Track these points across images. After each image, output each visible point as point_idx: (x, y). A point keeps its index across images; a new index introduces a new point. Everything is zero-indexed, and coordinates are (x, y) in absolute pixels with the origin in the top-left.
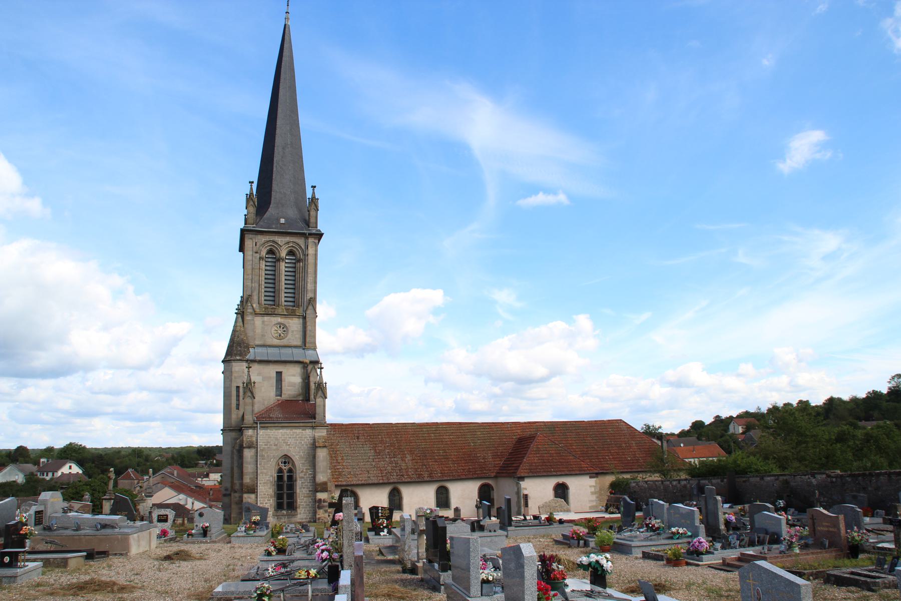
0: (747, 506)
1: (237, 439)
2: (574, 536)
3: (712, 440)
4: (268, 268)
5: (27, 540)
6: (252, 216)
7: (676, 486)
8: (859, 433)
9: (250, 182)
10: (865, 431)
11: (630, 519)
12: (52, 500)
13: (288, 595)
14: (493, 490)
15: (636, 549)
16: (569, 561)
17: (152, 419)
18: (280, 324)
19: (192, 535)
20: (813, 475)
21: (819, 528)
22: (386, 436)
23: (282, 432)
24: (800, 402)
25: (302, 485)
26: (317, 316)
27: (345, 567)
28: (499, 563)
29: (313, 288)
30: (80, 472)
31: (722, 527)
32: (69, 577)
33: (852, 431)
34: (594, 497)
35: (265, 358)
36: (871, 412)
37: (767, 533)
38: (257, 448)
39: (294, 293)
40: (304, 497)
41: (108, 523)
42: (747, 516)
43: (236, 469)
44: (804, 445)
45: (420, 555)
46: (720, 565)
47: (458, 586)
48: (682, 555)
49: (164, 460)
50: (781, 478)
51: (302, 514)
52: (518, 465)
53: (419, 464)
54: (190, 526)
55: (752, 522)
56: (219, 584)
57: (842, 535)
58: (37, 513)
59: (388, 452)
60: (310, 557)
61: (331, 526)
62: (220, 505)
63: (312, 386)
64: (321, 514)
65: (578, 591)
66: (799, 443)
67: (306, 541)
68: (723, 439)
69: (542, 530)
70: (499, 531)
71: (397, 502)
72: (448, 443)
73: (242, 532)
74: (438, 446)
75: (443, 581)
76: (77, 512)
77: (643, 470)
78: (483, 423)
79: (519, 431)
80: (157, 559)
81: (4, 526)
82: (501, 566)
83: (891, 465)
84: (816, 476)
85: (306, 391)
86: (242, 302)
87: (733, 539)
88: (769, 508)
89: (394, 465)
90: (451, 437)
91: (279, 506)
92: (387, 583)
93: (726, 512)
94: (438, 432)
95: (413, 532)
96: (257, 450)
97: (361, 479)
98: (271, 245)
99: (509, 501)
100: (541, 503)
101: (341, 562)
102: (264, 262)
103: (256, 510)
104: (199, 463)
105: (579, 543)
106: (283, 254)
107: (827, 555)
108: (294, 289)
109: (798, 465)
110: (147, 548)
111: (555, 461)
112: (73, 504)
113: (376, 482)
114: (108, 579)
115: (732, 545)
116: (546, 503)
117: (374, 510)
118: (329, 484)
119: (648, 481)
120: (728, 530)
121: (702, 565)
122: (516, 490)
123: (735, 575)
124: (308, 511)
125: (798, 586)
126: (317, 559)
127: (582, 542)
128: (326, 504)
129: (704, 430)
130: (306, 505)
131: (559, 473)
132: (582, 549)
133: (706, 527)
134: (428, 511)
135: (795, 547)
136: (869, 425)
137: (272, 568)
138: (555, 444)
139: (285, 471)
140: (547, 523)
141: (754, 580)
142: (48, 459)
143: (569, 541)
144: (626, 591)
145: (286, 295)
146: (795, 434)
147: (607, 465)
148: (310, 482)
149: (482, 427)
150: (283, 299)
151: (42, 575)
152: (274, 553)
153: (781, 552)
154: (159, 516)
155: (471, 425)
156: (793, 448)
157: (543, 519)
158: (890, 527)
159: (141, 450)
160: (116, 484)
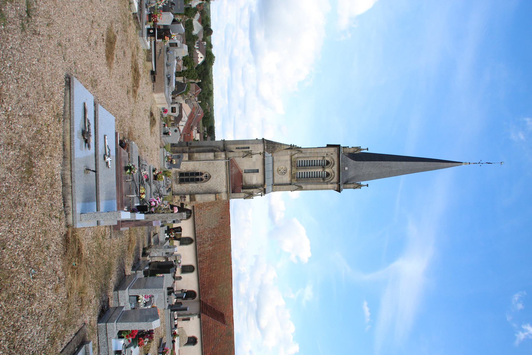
1: (219, 148)
5: (161, 40)
6: (348, 151)
12: (183, 51)
13: (130, 183)
14: (193, 299)
16: (150, 348)
17: (229, 99)
18: (286, 170)
25: (193, 187)
28: (149, 305)
29: (308, 189)
30: (199, 63)
32: (142, 63)
35: (266, 163)
38: (214, 160)
39: (305, 178)
40: (187, 188)
43: (202, 149)
45: (154, 258)
49: (207, 108)
51: (177, 187)
52: (208, 314)
58: (176, 44)
60: (152, 194)
61: (170, 205)
62: (182, 140)
63: (251, 191)
64: (177, 198)
67: (161, 191)
69: (168, 330)
71: (185, 242)
72: (220, 272)
73: (167, 154)
74: (218, 266)
76: (177, 64)
78: (232, 292)
79: (228, 314)
80: (151, 109)
85: (248, 187)
86: (298, 148)
89: (206, 240)
90: (223, 273)
91: (181, 174)
92: (137, 239)
94: (226, 265)
96: (213, 160)
97: (198, 220)
100: (184, 328)
101: (149, 213)
102: (321, 159)
106: (327, 170)
108: (307, 177)
113: (196, 229)
114: (140, 84)
116: (185, 332)
117: (179, 229)
118: (194, 202)
122: (193, 313)
131: (203, 339)
134: (179, 261)
137: (146, 173)
138: (220, 337)
139: (201, 177)
140: (172, 333)
142: (206, 46)
148: (195, 191)
149: (230, 292)
150: (301, 171)
151: (143, 49)
152: (154, 173)
154: (175, 108)
155: (231, 285)
159: (212, 95)
160: (192, 83)
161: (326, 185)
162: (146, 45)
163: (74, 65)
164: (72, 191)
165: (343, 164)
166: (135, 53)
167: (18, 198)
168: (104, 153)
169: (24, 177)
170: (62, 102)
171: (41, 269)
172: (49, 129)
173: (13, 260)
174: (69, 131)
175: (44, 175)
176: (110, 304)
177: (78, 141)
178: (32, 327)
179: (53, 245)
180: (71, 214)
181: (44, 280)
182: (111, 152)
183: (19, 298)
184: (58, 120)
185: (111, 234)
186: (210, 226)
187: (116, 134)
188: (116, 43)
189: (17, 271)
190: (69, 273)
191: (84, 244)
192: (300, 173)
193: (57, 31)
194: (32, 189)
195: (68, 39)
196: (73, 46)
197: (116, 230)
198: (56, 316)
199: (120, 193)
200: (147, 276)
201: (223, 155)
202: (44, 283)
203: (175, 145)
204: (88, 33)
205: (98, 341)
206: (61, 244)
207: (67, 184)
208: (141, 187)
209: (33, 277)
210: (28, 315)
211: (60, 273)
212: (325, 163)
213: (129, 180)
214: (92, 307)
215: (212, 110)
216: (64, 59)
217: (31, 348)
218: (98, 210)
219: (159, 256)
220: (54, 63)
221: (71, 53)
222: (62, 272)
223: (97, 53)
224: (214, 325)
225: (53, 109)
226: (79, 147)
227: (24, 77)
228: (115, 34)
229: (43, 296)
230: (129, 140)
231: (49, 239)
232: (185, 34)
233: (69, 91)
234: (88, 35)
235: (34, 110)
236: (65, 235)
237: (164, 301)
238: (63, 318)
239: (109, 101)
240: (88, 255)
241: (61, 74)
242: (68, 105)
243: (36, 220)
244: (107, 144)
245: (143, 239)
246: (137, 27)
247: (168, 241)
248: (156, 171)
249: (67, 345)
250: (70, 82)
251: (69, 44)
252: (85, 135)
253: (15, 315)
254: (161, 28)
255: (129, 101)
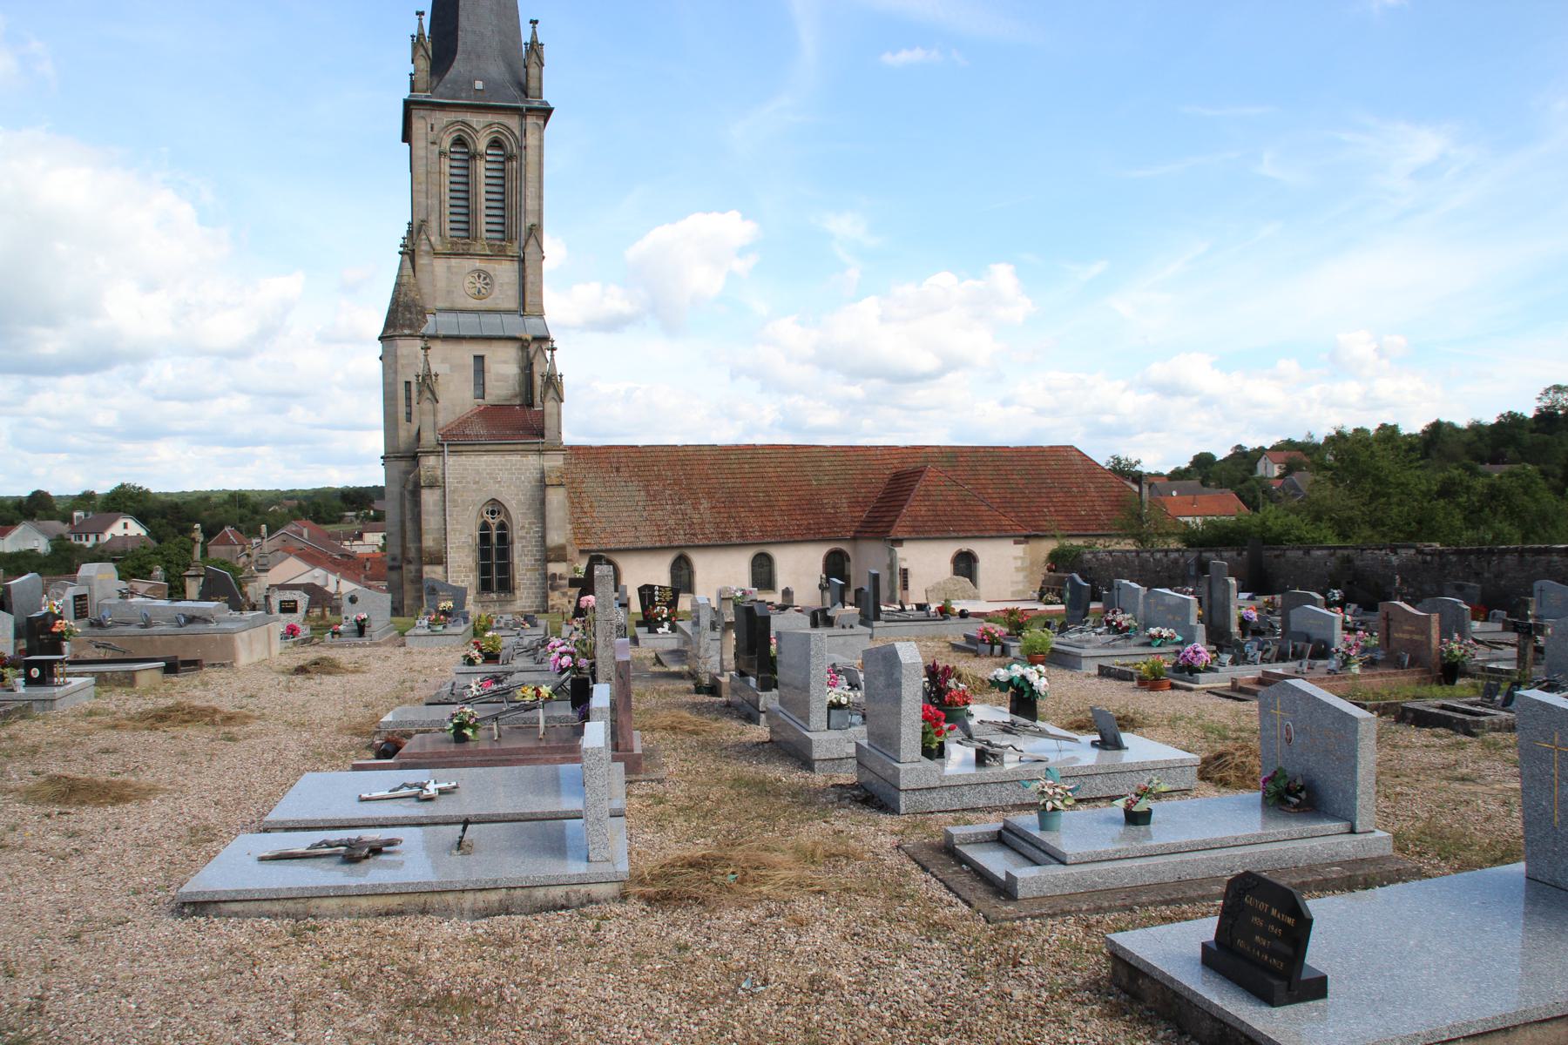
0: (1278, 597)
1: (408, 473)
2: (985, 637)
3: (1226, 487)
4: (455, 171)
5: (65, 643)
6: (424, 77)
7: (1160, 560)
8: (1479, 484)
9: (417, 14)
10: (1487, 481)
11: (1080, 612)
12: (100, 578)
13: (505, 728)
14: (849, 560)
15: (1089, 660)
16: (975, 678)
17: (256, 441)
19: (339, 633)
20: (1394, 550)
21: (1396, 635)
22: (666, 468)
23: (486, 461)
24: (1383, 427)
26: (544, 258)
27: (599, 680)
28: (857, 677)
29: (537, 208)
30: (143, 533)
31: (1235, 629)
32: (140, 701)
33: (1467, 478)
34: (1020, 576)
35: (455, 333)
36: (1502, 449)
37: (1308, 640)
39: (503, 216)
40: (527, 570)
41: (197, 615)
42: (1276, 613)
43: (409, 525)
44: (1383, 500)
45: (725, 663)
46: (1228, 690)
47: (789, 714)
48: (1165, 672)
49: (285, 510)
50: (1340, 553)
51: (524, 599)
52: (893, 518)
53: (722, 515)
54: (334, 619)
55: (1286, 623)
56: (388, 710)
57: (1433, 646)
58: (79, 598)
59: (670, 495)
60: (539, 667)
61: (574, 617)
62: (383, 585)
63: (538, 381)
64: (556, 599)
65: (990, 723)
66: (1375, 496)
67: (532, 642)
68: (1246, 484)
69: (931, 628)
70: (859, 626)
71: (685, 579)
72: (774, 479)
74: (757, 485)
75: (765, 706)
76: (143, 596)
77: (1105, 533)
78: (833, 447)
79: (895, 461)
80: (283, 672)
81: (25, 620)
82: (863, 683)
83: (1525, 539)
84: (1399, 551)
86: (410, 232)
87: (1251, 647)
88: (1316, 599)
89: (680, 516)
90: (779, 470)
91: (485, 586)
92: (669, 709)
93: (1242, 605)
94: (756, 461)
95: (713, 627)
96: (444, 492)
97: (623, 540)
98: (460, 130)
99: (875, 579)
100: (929, 585)
101: (593, 674)
103: (446, 590)
104: (344, 516)
105: (992, 649)
106: (482, 145)
107: (1405, 679)
108: (503, 209)
109: (1370, 533)
110: (266, 655)
111: (955, 513)
112: (136, 585)
113: (649, 545)
114: (205, 704)
115: (1249, 659)
116: (939, 583)
117: (646, 592)
118: (569, 549)
119: (1113, 551)
120: (1244, 635)
121: (1197, 690)
122: (888, 561)
123: (1253, 706)
124: (533, 593)
125: (1354, 720)
126: (552, 668)
127: (997, 648)
128: (566, 582)
129: (1215, 468)
130: (531, 584)
131: (961, 534)
132: (997, 660)
133: (1207, 628)
134: (739, 594)
135: (1354, 664)
136: (1496, 472)
137: (477, 683)
138: (958, 485)
139: (494, 527)
140: (939, 616)
141: (1283, 710)
142: (86, 511)
143: (973, 646)
144: (1069, 727)
145: (489, 220)
146: (1370, 480)
147: (1045, 523)
148: (536, 546)
150: (484, 227)
151: (96, 697)
152: (479, 661)
153: (1330, 672)
154: (281, 602)
155: (813, 450)
156: (1364, 505)
157: (933, 609)
158: (1513, 637)
159: (243, 495)
160: (205, 552)
161: (529, 151)
162: (82, 689)
163: (143, 895)
164: (522, 887)
165: (463, 95)
166: (108, 720)
167: (539, 1031)
168: (413, 802)
169: (478, 1017)
170: (256, 925)
171: (742, 963)
172: (337, 956)
173: (714, 1037)
174: (346, 901)
175: (475, 965)
176: (849, 782)
177: (375, 874)
178: (898, 980)
179: (675, 935)
180: (590, 887)
181: (771, 955)
182: (411, 781)
183: (817, 1017)
184: (311, 933)
185: (652, 781)
186: (640, 504)
187: (356, 768)
188: (72, 775)
189: (743, 1025)
190: (756, 889)
191: (674, 851)
192: (487, 231)
193: (33, 947)
194: (513, 994)
195: (58, 916)
196: (80, 900)
197: (639, 764)
198: (874, 921)
199: (532, 756)
200: (776, 681)
201: (429, 462)
202: (780, 955)
203: (396, 605)
204: (40, 857)
205: (946, 811)
206: (673, 912)
207: (501, 901)
208: (517, 698)
209: (763, 985)
210: (865, 993)
211: (757, 913)
212: (459, 149)
213: (496, 731)
214: (853, 828)
215: (291, 495)
216: (121, 923)
217: (954, 981)
218: (577, 816)
219: (721, 648)
220: (137, 951)
221: (103, 905)
222: (752, 910)
223: (104, 830)
224: (925, 501)
225: (278, 947)
226: (392, 872)
227: (178, 1032)
228: (43, 780)
229: (818, 955)
230: (376, 733)
231: (659, 947)
232: (50, 575)
233: (221, 905)
234: (45, 858)
235: (280, 998)
236: (649, 904)
237: (848, 638)
238: (880, 903)
239: (255, 791)
240: (710, 840)
241: (171, 929)
242: (267, 906)
243: (603, 982)
244: (385, 793)
245: (670, 694)
246: (23, 717)
247: (678, 623)
248: (472, 656)
249: (954, 892)
250: (194, 903)
251: (76, 910)
252: (357, 854)
253: (864, 1024)
254: (25, 647)
255: (257, 735)
